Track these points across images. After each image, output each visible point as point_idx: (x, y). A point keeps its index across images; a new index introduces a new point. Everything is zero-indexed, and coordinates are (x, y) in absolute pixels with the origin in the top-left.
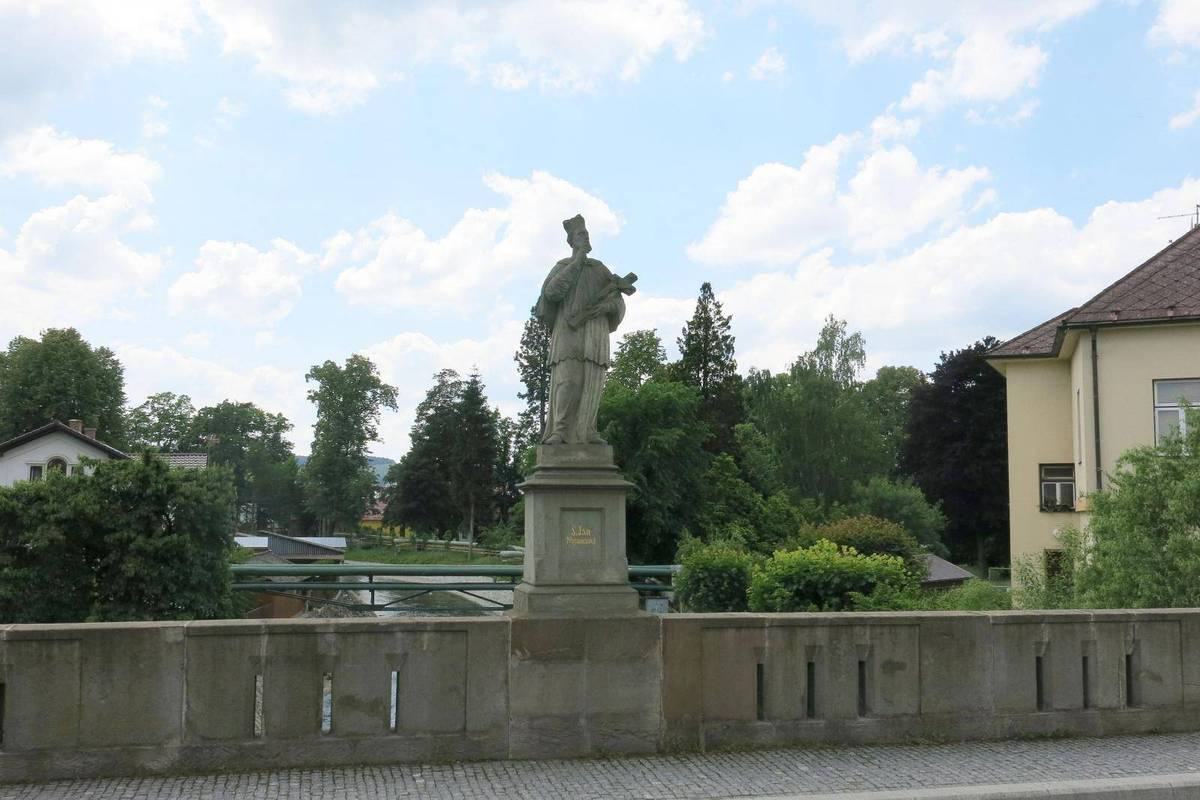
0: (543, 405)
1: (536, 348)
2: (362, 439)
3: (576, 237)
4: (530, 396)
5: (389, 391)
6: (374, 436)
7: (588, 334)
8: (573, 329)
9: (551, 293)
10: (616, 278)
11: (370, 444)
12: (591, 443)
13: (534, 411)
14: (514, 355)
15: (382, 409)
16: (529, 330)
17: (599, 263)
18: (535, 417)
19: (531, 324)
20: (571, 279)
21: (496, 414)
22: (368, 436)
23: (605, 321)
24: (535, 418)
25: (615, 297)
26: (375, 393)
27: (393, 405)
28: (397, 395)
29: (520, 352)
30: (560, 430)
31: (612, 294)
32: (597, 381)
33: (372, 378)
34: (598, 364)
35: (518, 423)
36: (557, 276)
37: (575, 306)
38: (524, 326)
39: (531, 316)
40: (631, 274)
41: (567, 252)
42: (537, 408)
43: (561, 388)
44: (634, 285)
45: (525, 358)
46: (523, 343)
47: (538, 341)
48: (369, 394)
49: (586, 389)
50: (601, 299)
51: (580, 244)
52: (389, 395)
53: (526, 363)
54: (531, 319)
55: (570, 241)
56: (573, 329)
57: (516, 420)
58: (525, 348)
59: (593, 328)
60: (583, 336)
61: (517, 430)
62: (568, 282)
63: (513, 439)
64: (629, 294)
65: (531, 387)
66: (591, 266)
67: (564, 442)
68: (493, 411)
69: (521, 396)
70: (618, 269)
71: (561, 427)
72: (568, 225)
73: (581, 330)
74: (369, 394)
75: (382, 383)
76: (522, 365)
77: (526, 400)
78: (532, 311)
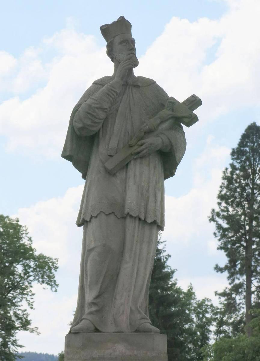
0: (249, 282)
1: (239, 204)
2: (9, 328)
3: (117, 47)
4: (231, 269)
5: (46, 263)
6: (25, 324)
7: (131, 183)
8: (111, 173)
9: (80, 125)
10: (173, 102)
11: (20, 335)
12: (137, 331)
13: (236, 289)
14: (210, 215)
15: (37, 288)
16: (230, 180)
17: (151, 84)
18: (238, 298)
19: (232, 173)
20: (106, 106)
21: (190, 294)
22: (17, 324)
23: (156, 163)
24: (239, 299)
25: (171, 128)
26: (26, 267)
27: (51, 281)
28: (56, 268)
29: (217, 209)
30: (91, 313)
31: (165, 125)
32: (145, 247)
33: (24, 245)
34: (145, 221)
35: (220, 306)
36: (89, 101)
37: (114, 143)
38: (222, 175)
39: (231, 161)
40: (194, 96)
41: (106, 68)
42: (240, 285)
43: (93, 254)
44: (195, 112)
45: (224, 218)
46: (222, 197)
47: (241, 196)
48: (19, 268)
49: (127, 256)
50: (149, 132)
51: (122, 56)
52: (45, 268)
53: (225, 225)
54: (232, 166)
55: (111, 53)
56: (111, 173)
57: (218, 303)
58: (224, 204)
59: (141, 171)
60: (125, 182)
61: (218, 316)
62: (102, 109)
63: (213, 328)
64: (188, 125)
65: (232, 255)
66: (137, 86)
67: (97, 330)
68: (185, 289)
69: (218, 269)
70: (179, 93)
71: (93, 309)
72: (106, 31)
73: (121, 175)
74: (19, 268)
75: (37, 254)
76: (219, 227)
77: (226, 274)
78: (233, 154)
